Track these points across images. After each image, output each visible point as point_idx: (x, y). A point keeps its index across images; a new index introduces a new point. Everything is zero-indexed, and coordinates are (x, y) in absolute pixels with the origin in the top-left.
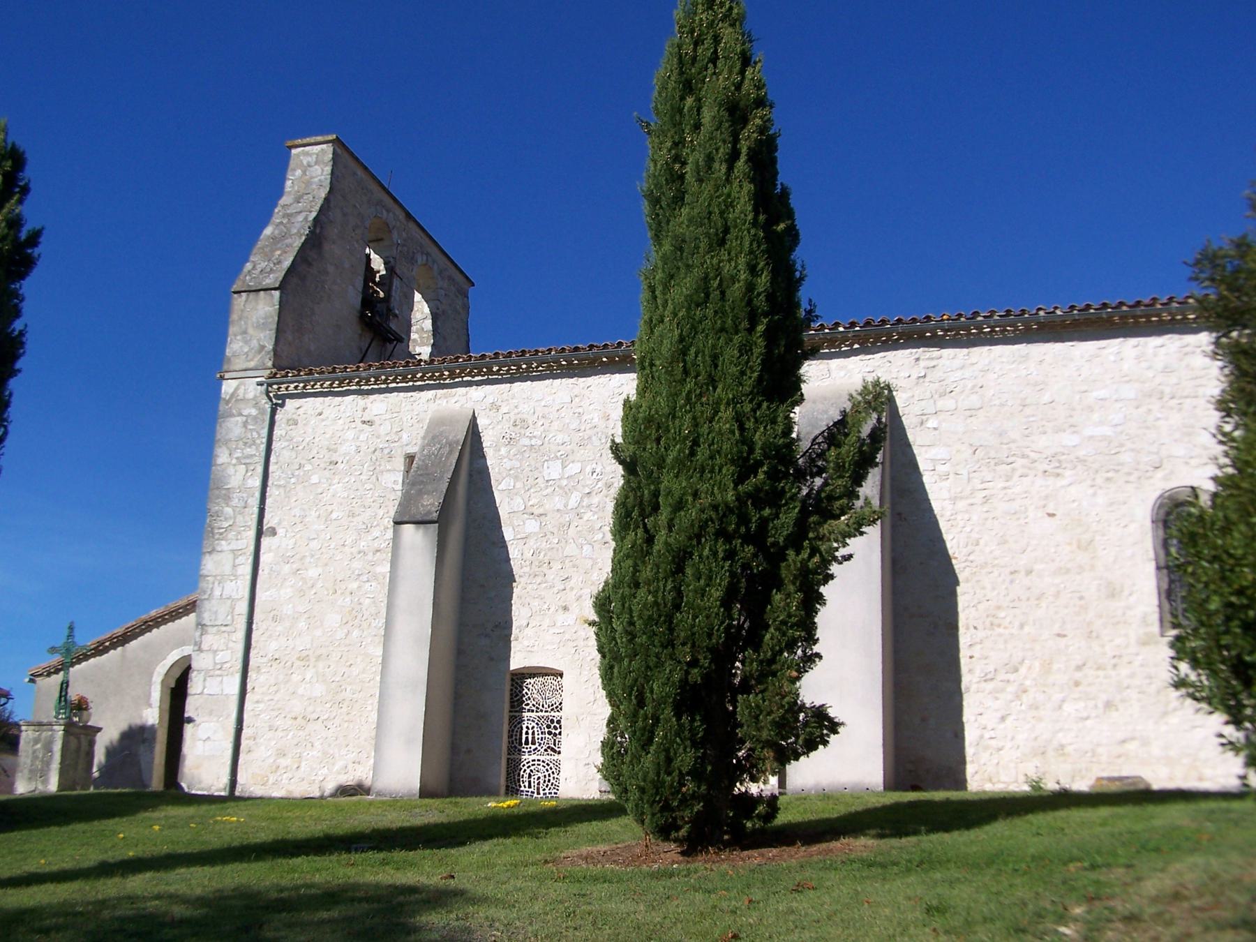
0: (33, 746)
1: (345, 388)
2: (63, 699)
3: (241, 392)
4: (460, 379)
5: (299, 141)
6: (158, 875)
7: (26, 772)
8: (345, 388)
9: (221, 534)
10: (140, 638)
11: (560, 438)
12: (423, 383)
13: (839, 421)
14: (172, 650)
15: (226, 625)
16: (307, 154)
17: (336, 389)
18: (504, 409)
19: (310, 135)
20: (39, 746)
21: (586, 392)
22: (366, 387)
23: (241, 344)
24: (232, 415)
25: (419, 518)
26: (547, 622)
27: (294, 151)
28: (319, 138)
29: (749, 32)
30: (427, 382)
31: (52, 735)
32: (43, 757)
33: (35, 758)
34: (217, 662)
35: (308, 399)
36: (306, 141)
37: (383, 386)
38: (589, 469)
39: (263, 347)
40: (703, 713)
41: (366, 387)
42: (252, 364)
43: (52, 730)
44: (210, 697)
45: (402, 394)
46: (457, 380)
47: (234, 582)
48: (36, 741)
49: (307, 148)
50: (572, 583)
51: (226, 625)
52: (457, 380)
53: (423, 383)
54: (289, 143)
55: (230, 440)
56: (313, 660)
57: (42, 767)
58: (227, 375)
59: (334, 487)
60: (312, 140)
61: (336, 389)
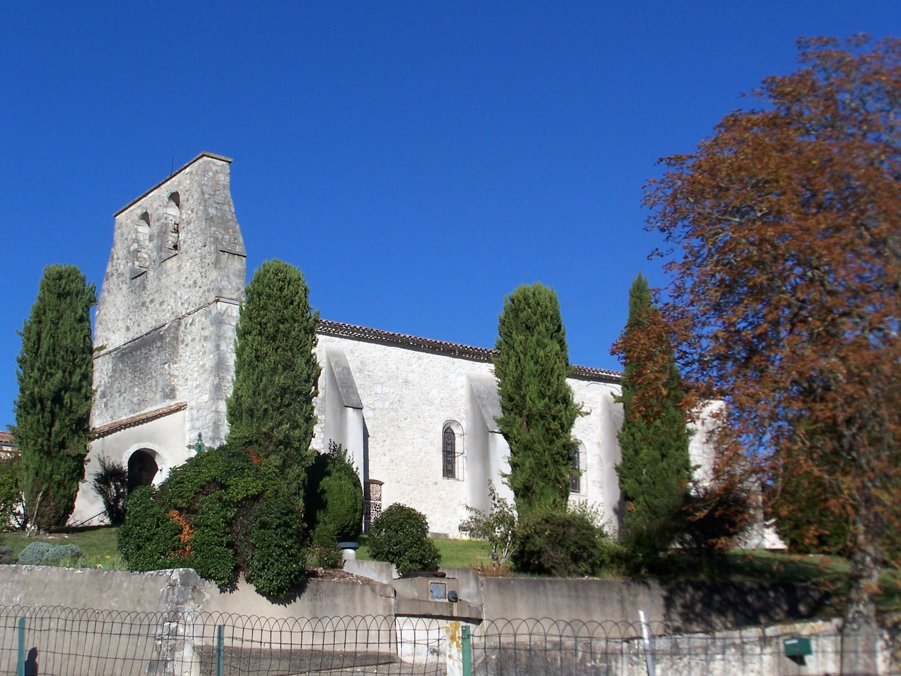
3: (229, 311)
6: (541, 578)
11: (380, 374)
13: (624, 407)
16: (214, 164)
18: (356, 354)
21: (389, 354)
23: (741, 348)
24: (226, 324)
25: (355, 406)
26: (377, 460)
28: (223, 158)
29: (645, 204)
36: (211, 155)
38: (392, 391)
39: (239, 289)
42: (234, 297)
50: (387, 443)
55: (226, 337)
58: (221, 299)
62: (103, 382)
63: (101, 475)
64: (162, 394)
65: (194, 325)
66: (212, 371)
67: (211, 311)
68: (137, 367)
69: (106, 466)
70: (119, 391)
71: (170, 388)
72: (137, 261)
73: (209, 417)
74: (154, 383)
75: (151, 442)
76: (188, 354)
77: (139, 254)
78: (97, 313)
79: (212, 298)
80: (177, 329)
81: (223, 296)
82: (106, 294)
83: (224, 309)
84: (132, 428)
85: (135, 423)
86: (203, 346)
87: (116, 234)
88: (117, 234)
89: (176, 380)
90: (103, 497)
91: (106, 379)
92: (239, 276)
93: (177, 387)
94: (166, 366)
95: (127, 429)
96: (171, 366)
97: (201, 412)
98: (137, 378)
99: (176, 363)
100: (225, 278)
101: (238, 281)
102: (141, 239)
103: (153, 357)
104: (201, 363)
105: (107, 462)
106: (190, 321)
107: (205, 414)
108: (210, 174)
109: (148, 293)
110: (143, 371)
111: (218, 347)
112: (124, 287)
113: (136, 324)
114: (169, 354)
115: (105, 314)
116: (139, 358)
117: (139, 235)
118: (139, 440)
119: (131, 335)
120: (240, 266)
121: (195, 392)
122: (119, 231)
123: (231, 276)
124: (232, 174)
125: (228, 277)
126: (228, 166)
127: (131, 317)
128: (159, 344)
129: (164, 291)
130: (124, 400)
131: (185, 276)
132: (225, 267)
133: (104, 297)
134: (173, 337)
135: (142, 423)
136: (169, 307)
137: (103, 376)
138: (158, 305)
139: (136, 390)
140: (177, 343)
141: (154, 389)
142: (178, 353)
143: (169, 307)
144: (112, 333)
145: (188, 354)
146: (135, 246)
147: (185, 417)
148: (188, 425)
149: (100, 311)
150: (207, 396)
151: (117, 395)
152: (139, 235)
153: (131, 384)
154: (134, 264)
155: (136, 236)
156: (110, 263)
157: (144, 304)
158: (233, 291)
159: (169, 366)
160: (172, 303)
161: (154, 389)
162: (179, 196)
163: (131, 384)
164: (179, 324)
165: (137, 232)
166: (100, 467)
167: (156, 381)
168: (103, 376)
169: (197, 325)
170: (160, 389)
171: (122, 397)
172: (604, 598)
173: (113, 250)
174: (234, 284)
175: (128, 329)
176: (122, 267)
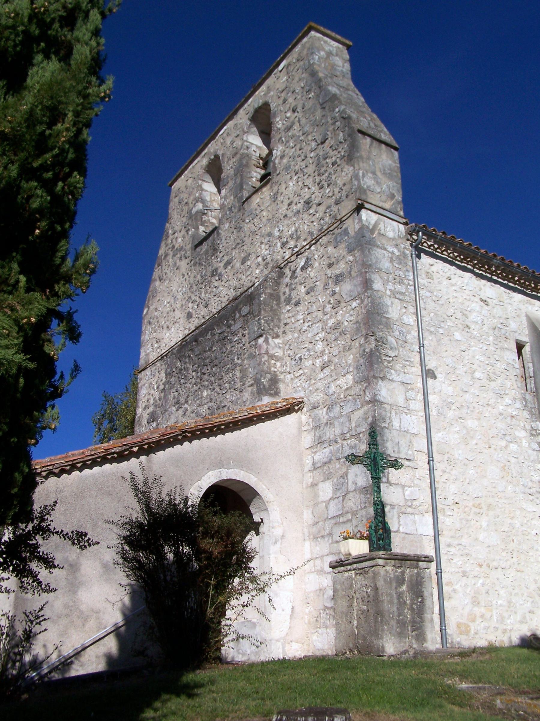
0: (396, 588)
1: (463, 264)
2: (341, 520)
4: (536, 294)
5: (322, 28)
7: (393, 623)
8: (463, 264)
9: (389, 362)
10: (169, 450)
12: (513, 285)
14: (209, 470)
15: (409, 460)
16: (325, 42)
17: (457, 262)
19: (325, 27)
20: (404, 588)
22: (477, 271)
24: (378, 247)
27: (313, 33)
28: (339, 37)
30: (516, 286)
31: (418, 574)
32: (412, 604)
33: (402, 604)
34: (407, 498)
35: (438, 261)
37: (489, 275)
40: (166, 562)
41: (477, 271)
43: (417, 567)
44: (406, 536)
45: (502, 288)
46: (534, 293)
47: (409, 415)
48: (400, 581)
49: (326, 39)
51: (409, 460)
52: (534, 293)
53: (513, 285)
54: (313, 24)
56: (485, 508)
57: (413, 618)
59: (476, 348)
60: (333, 34)
61: (457, 262)
62: (152, 401)
63: (140, 525)
64: (255, 388)
65: (311, 266)
66: (358, 329)
67: (346, 229)
68: (205, 359)
69: (153, 506)
70: (177, 402)
71: (268, 376)
72: (202, 225)
73: (360, 413)
74: (238, 374)
75: (241, 468)
76: (300, 317)
77: (205, 218)
78: (145, 311)
79: (349, 205)
80: (277, 284)
81: (369, 201)
82: (157, 283)
83: (373, 222)
84: (204, 440)
85: (211, 429)
86: (334, 293)
87: (171, 205)
88: (174, 203)
89: (278, 364)
90: (482, 648)
91: (157, 395)
92: (390, 177)
93: (281, 377)
94: (261, 341)
95: (195, 442)
96: (270, 340)
97: (337, 409)
98: (206, 377)
99: (277, 336)
100: (370, 175)
101: (390, 183)
102: (208, 198)
103: (234, 334)
104: (331, 323)
105: (154, 496)
106: (302, 264)
107: (347, 409)
108: (322, 53)
109: (221, 255)
110: (216, 362)
111: (367, 284)
112: (183, 264)
113: (201, 306)
114: (266, 321)
115: (156, 310)
116: (209, 343)
117: (204, 192)
118: (219, 464)
119: (195, 323)
120: (390, 162)
121: (322, 375)
122: (176, 200)
123: (379, 174)
124: (352, 61)
125: (374, 173)
126: (346, 52)
127: (193, 298)
128: (245, 310)
129: (247, 241)
130: (184, 415)
131: (286, 202)
132: (368, 158)
133: (155, 288)
134: (271, 295)
135: (223, 432)
136: (260, 259)
137: (152, 392)
138: (238, 265)
139: (205, 394)
140: (278, 305)
141: (238, 385)
142: (279, 320)
143: (260, 259)
144: (165, 330)
145: (300, 317)
146: (200, 206)
147: (300, 424)
148: (308, 439)
149: (149, 307)
150: (350, 377)
151: (174, 409)
152: (204, 192)
153: (195, 388)
154: (197, 228)
155: (201, 194)
156: (164, 242)
157: (215, 272)
158: (384, 198)
159: (266, 341)
160: (264, 252)
161: (238, 385)
162: (269, 105)
163: (195, 388)
164: (281, 275)
165: (202, 190)
166: (137, 506)
167: (241, 371)
168: (152, 392)
169: (316, 264)
170: (251, 381)
171: (181, 412)
172: (458, 644)
173: (167, 225)
174: (385, 186)
175: (189, 316)
176: (180, 240)
